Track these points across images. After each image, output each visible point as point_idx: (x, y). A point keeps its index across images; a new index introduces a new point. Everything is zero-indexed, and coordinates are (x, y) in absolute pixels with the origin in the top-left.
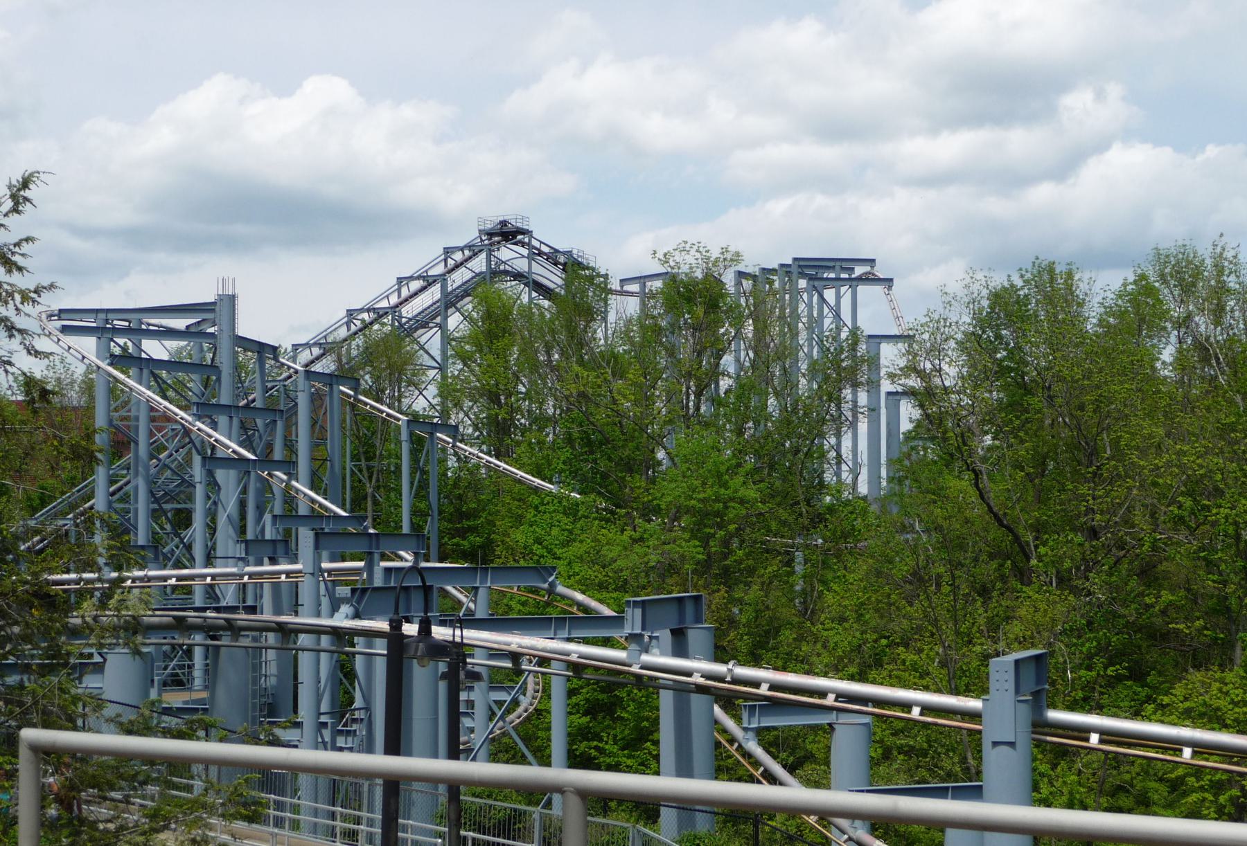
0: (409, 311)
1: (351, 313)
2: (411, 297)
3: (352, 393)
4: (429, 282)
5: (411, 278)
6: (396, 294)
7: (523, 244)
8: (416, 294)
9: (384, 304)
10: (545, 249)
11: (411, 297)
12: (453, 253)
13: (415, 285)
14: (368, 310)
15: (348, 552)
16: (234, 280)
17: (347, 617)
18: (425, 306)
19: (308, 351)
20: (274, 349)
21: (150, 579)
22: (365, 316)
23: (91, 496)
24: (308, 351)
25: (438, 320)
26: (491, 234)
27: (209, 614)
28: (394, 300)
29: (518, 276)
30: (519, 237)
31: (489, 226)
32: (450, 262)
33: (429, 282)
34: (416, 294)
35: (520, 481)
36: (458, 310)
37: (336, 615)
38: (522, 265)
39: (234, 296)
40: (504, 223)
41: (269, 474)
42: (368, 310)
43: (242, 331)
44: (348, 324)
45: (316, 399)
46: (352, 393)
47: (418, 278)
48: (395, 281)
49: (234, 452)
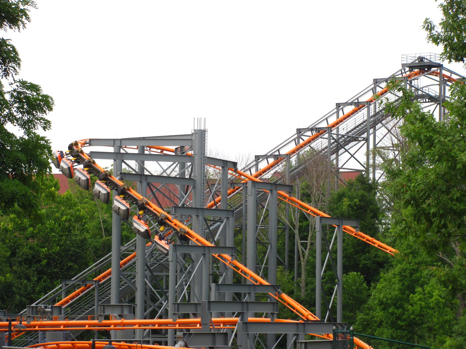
0: (344, 128)
1: (300, 132)
2: (345, 118)
3: (287, 195)
4: (359, 106)
5: (347, 104)
6: (335, 116)
7: (436, 74)
8: (349, 116)
9: (324, 125)
10: (454, 77)
11: (345, 118)
12: (380, 83)
13: (348, 109)
14: (312, 130)
15: (226, 312)
16: (205, 119)
17: (181, 346)
18: (357, 124)
19: (265, 161)
20: (235, 164)
21: (124, 325)
22: (309, 133)
23: (109, 266)
24: (265, 161)
25: (365, 135)
26: (412, 67)
27: (122, 343)
28: (333, 120)
29: (432, 99)
30: (433, 69)
31: (410, 61)
32: (341, 115)
33: (359, 106)
34: (349, 116)
35: (73, 319)
36: (383, 125)
37: (176, 345)
38: (435, 91)
39: (204, 131)
40: (421, 59)
41: (219, 256)
42: (312, 130)
43: (208, 154)
44: (374, 90)
45: (259, 203)
46: (287, 195)
47: (351, 104)
48: (335, 106)
49: (197, 240)
